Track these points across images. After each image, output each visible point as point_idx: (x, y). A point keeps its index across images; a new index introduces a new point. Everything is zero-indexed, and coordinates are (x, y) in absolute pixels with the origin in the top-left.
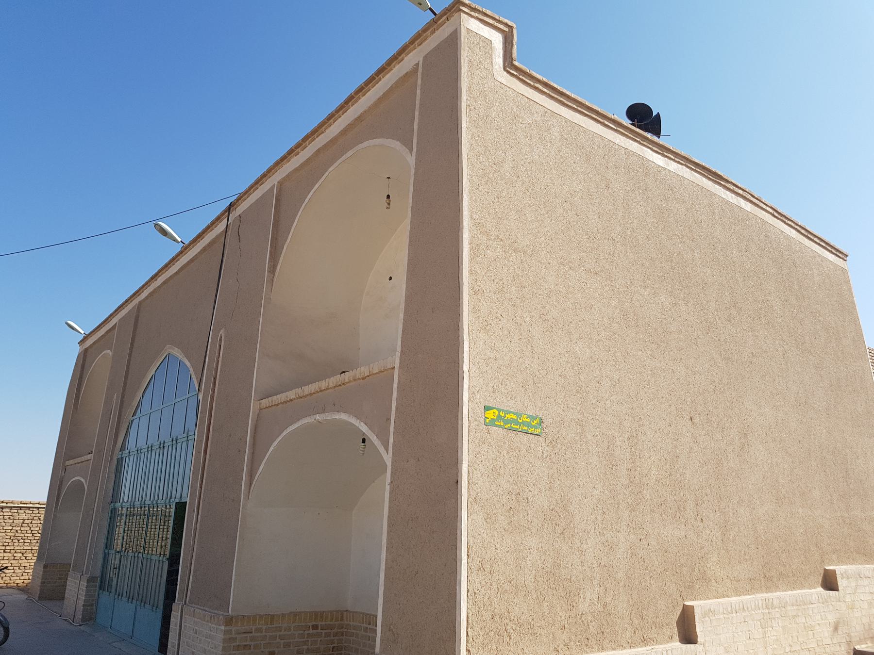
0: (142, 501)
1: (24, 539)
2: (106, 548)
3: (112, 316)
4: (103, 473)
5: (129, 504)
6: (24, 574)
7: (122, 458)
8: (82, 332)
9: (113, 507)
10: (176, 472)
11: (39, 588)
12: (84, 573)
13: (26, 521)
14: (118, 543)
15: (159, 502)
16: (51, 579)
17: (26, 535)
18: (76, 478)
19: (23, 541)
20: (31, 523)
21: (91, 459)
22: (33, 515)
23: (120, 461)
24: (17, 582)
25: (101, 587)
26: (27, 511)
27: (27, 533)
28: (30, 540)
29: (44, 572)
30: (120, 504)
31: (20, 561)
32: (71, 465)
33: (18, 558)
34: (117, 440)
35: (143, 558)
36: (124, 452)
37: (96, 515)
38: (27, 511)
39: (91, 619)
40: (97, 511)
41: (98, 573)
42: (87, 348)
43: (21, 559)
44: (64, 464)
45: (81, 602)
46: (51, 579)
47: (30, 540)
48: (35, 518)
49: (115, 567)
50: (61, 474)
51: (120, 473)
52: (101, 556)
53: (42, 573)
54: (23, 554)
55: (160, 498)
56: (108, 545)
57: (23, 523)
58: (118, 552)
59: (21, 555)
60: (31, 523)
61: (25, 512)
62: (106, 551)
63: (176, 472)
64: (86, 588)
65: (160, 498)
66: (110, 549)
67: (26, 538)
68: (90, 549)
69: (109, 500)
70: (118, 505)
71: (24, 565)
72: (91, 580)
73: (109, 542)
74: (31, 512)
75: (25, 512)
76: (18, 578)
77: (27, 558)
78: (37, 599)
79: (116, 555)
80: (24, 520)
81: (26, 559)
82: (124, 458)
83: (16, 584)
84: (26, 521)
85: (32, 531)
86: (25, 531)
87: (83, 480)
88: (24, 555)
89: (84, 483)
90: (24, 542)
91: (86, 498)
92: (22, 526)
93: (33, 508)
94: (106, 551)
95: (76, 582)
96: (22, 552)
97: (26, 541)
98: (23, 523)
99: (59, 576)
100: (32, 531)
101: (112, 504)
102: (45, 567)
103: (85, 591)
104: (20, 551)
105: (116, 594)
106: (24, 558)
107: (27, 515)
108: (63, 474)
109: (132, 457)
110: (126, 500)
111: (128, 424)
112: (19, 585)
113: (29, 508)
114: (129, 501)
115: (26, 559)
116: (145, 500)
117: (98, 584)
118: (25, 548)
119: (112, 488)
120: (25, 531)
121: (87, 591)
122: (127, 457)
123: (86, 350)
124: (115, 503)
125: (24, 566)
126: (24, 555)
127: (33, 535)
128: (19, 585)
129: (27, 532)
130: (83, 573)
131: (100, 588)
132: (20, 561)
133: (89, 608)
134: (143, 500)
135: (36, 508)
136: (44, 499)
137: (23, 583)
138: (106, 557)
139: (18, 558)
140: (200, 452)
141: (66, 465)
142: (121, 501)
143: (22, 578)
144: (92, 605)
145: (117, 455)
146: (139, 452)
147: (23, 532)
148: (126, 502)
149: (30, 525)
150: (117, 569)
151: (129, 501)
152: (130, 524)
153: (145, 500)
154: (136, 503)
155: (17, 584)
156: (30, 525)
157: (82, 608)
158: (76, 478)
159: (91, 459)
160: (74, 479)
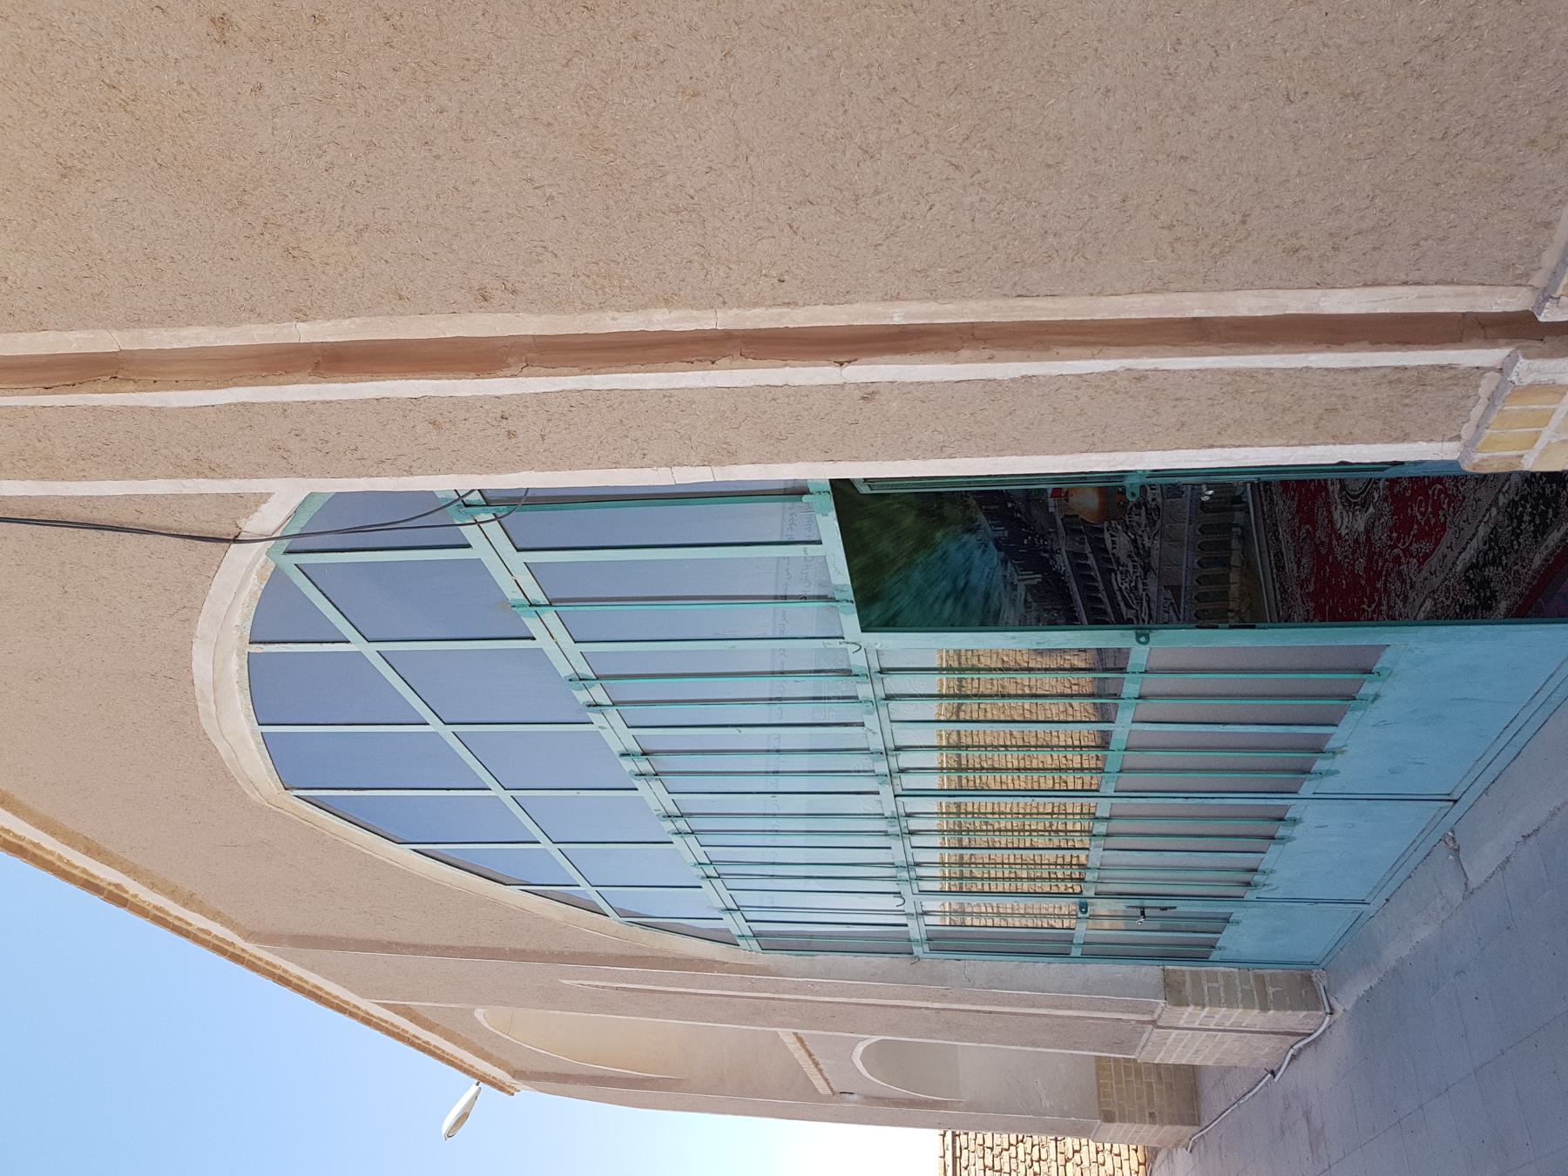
0: (886, 834)
1: (1032, 1161)
2: (1066, 955)
3: (367, 1020)
4: (817, 993)
5: (905, 889)
6: (1116, 1151)
7: (755, 935)
8: (474, 1089)
9: (926, 948)
10: (803, 762)
11: (1168, 1127)
12: (1147, 1018)
13: (989, 1162)
14: (1055, 913)
15: (876, 743)
16: (1139, 1098)
17: (1021, 1156)
18: (859, 1065)
19: (1036, 1164)
20: (992, 1149)
21: (795, 1034)
22: (972, 1148)
23: (770, 943)
24: (1135, 1166)
25: (1199, 954)
26: (964, 1163)
27: (1016, 1157)
28: (1033, 1146)
29: (1123, 1119)
30: (912, 924)
31: (1086, 1163)
32: (826, 1080)
33: (1078, 1169)
34: (701, 961)
35: (1121, 793)
36: (735, 931)
37: (959, 1001)
38: (964, 1163)
39: (1308, 979)
40: (943, 998)
41: (1151, 972)
42: (509, 1073)
43: (1079, 1163)
44: (827, 1099)
45: (1253, 1017)
46: (1139, 1098)
47: (1033, 1146)
48: (980, 1141)
49: (1138, 912)
50: (856, 1102)
51: (812, 936)
52: (1094, 969)
53: (1126, 1125)
54: (1067, 1160)
55: (882, 856)
56: (1056, 948)
57: (992, 1168)
58: (1083, 907)
59: (1069, 1165)
60: (992, 1149)
61: (966, 1168)
62: (1076, 952)
63: (803, 762)
64: (1204, 1006)
65: (882, 856)
66: (1071, 942)
67: (1028, 1157)
68: (1070, 1008)
69: (901, 962)
70: (915, 930)
71: (1093, 1155)
72: (1174, 993)
73: (1048, 947)
74: (965, 1152)
75: (966, 1168)
76: (1125, 1164)
77: (1077, 1148)
78: (1196, 1129)
79: (1094, 917)
80: (985, 1167)
81: (1079, 1151)
82: (757, 927)
83: (1141, 1167)
84: (989, 1162)
85: (1010, 1145)
86: (1013, 1161)
87: (860, 1048)
88: (1070, 1156)
89: (867, 1043)
90: (1040, 1160)
91: (906, 1034)
92: (1000, 1171)
93: (954, 1148)
94: (1076, 952)
95: (1175, 1040)
96: (1064, 1163)
97: (1036, 1157)
98: (992, 1168)
99: (1133, 1078)
100: (1010, 1145)
101: (917, 950)
102: (1108, 1117)
103: (1215, 1009)
104: (1061, 1169)
105: (1239, 898)
106: (1077, 1155)
107: (972, 1162)
108: (855, 1097)
109: (744, 899)
110: (891, 903)
111: (637, 928)
112: (1142, 1161)
113: (954, 1158)
114: (892, 887)
115: (1079, 1151)
116: (881, 816)
117: (1186, 968)
118: (1053, 1156)
119: (864, 958)
120: (1013, 1161)
121: (1215, 1002)
122: (750, 916)
123: (517, 1074)
124: (909, 940)
125: (1097, 1153)
126: (1070, 1156)
127: (1022, 1141)
128: (1142, 1161)
129: (1014, 1155)
130: (1150, 1022)
131: (1203, 958)
132: (1086, 1163)
133: (1270, 990)
134: (881, 825)
135: (954, 1142)
136: (933, 1135)
137: (1136, 1151)
138: (1098, 952)
139: (1078, 1169)
140: (505, 412)
141: (829, 1092)
142: (902, 920)
143: (1125, 1155)
144: (1260, 980)
145: (749, 954)
146: (710, 871)
147: (1014, 1167)
148: (901, 901)
149: (997, 1150)
150: (1147, 903)
151: (892, 887)
152: (966, 873)
153: (881, 816)
154: (900, 859)
155: (1139, 1164)
156: (997, 1150)
157: (1271, 1012)
158: (859, 1065)
159: (795, 1034)
160: (863, 1071)
